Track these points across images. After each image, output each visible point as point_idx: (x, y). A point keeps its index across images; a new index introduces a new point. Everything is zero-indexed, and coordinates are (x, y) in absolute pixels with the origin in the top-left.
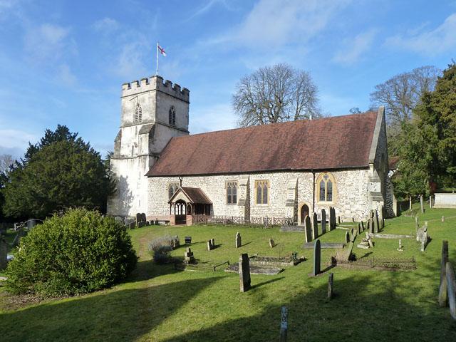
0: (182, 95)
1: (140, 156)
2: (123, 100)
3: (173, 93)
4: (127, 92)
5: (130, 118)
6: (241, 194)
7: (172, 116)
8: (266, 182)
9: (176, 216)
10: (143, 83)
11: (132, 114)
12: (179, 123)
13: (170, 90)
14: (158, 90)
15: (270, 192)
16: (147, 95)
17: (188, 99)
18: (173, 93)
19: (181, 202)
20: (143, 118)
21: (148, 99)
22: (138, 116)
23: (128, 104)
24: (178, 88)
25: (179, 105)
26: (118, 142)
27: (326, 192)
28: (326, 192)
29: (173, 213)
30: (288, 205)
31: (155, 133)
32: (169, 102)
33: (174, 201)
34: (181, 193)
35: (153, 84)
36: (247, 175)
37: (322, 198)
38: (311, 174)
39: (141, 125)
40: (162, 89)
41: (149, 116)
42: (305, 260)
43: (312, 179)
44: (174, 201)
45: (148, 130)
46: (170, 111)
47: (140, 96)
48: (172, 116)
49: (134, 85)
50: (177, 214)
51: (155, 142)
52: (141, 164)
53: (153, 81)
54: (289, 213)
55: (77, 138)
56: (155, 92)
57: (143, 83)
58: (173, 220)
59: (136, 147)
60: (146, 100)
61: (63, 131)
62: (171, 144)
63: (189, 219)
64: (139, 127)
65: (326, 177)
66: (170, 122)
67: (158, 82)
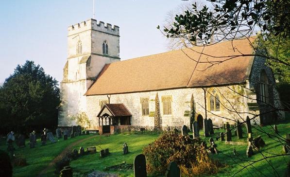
0: (114, 31)
1: (80, 80)
2: (69, 38)
3: (106, 30)
4: (72, 32)
5: (74, 51)
6: (152, 108)
7: (105, 47)
8: (169, 98)
9: (103, 126)
10: (82, 25)
11: (75, 48)
12: (111, 52)
13: (102, 28)
14: (92, 29)
15: (173, 105)
16: (85, 34)
17: (119, 33)
18: (106, 30)
19: (106, 115)
20: (83, 52)
21: (86, 38)
22: (80, 49)
23: (73, 42)
24: (109, 26)
25: (111, 39)
26: (66, 69)
27: (215, 104)
28: (215, 104)
29: (101, 125)
30: (186, 115)
31: (91, 62)
32: (103, 37)
33: (101, 115)
34: (106, 109)
35: (89, 25)
36: (156, 92)
37: (212, 108)
38: (201, 90)
39: (81, 57)
40: (96, 28)
41: (87, 50)
42: (193, 97)
43: (203, 94)
44: (101, 115)
45: (86, 60)
46: (104, 44)
47: (81, 35)
48: (105, 47)
49: (76, 27)
50: (104, 124)
51: (91, 69)
52: (82, 86)
53: (89, 23)
54: (187, 122)
55: (40, 67)
56: (90, 31)
57: (82, 25)
58: (101, 130)
59: (78, 73)
60: (85, 40)
61: (30, 64)
62: (90, 85)
63: (112, 131)
64: (80, 58)
65: (214, 92)
66: (104, 52)
67: (92, 24)
